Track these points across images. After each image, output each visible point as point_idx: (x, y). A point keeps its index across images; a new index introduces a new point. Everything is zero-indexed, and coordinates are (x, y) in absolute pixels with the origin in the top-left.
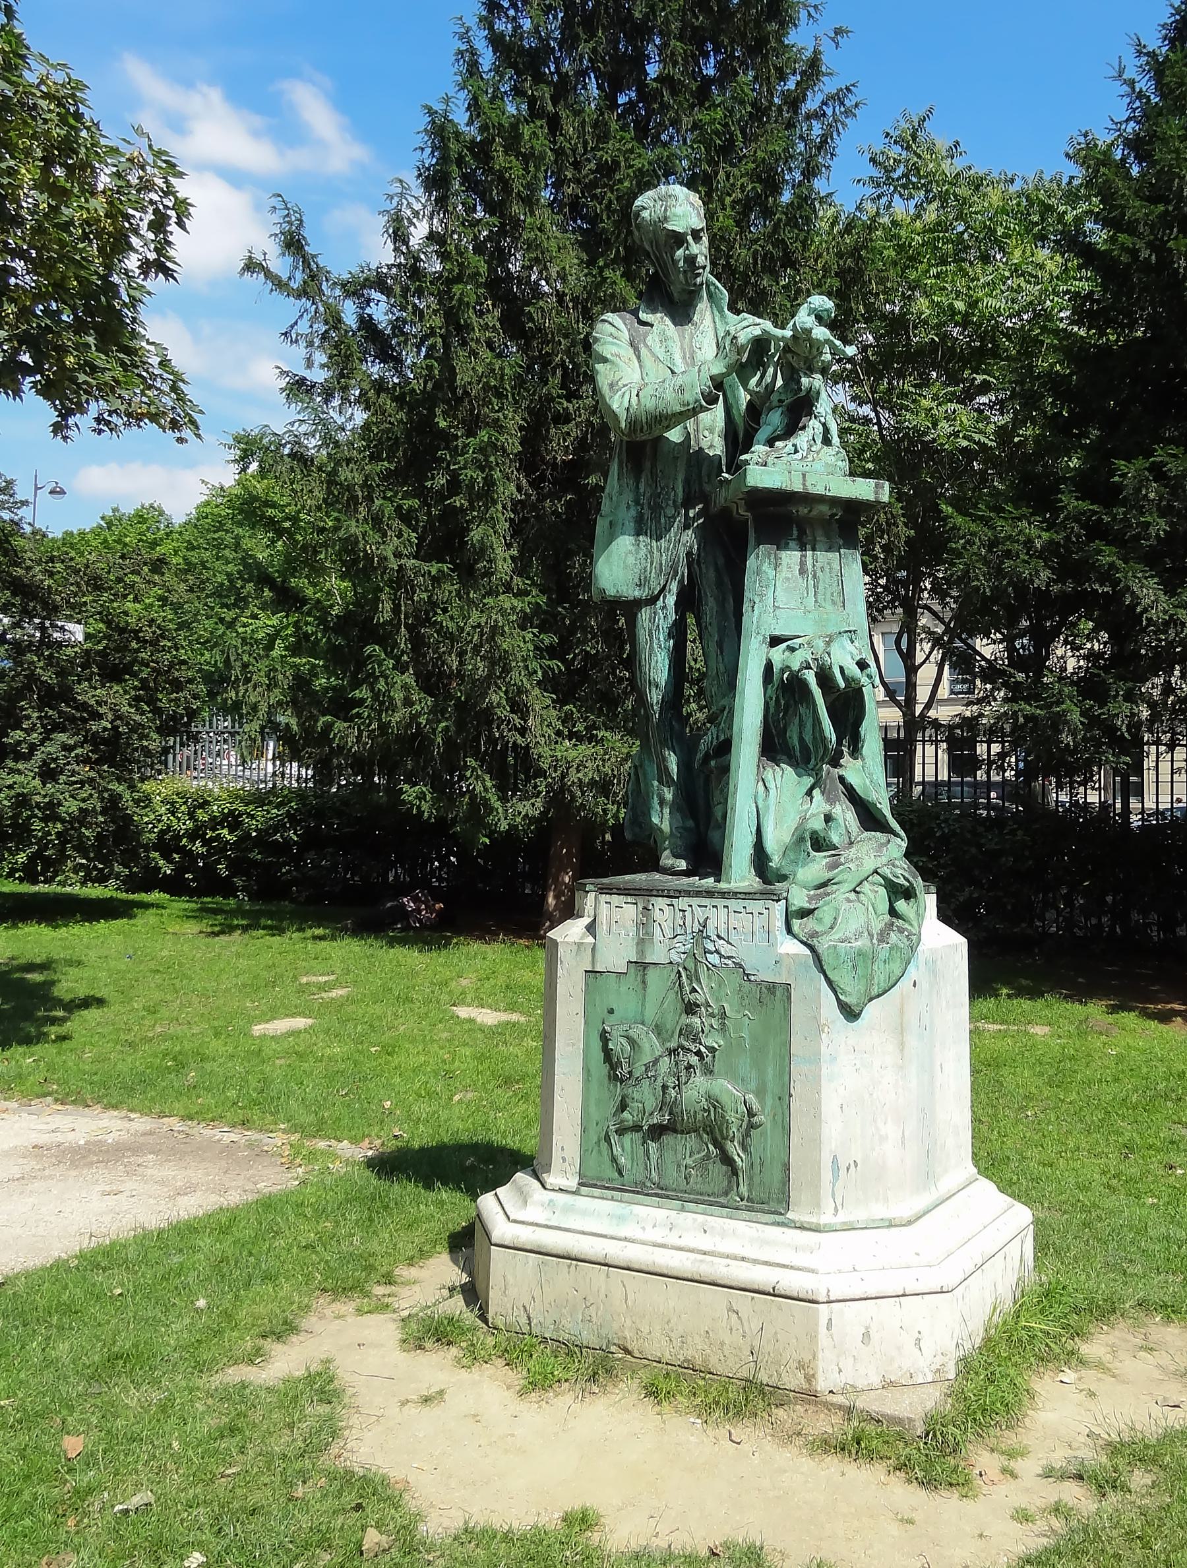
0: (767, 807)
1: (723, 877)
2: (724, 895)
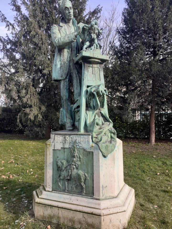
0: (87, 118)
2: (80, 135)
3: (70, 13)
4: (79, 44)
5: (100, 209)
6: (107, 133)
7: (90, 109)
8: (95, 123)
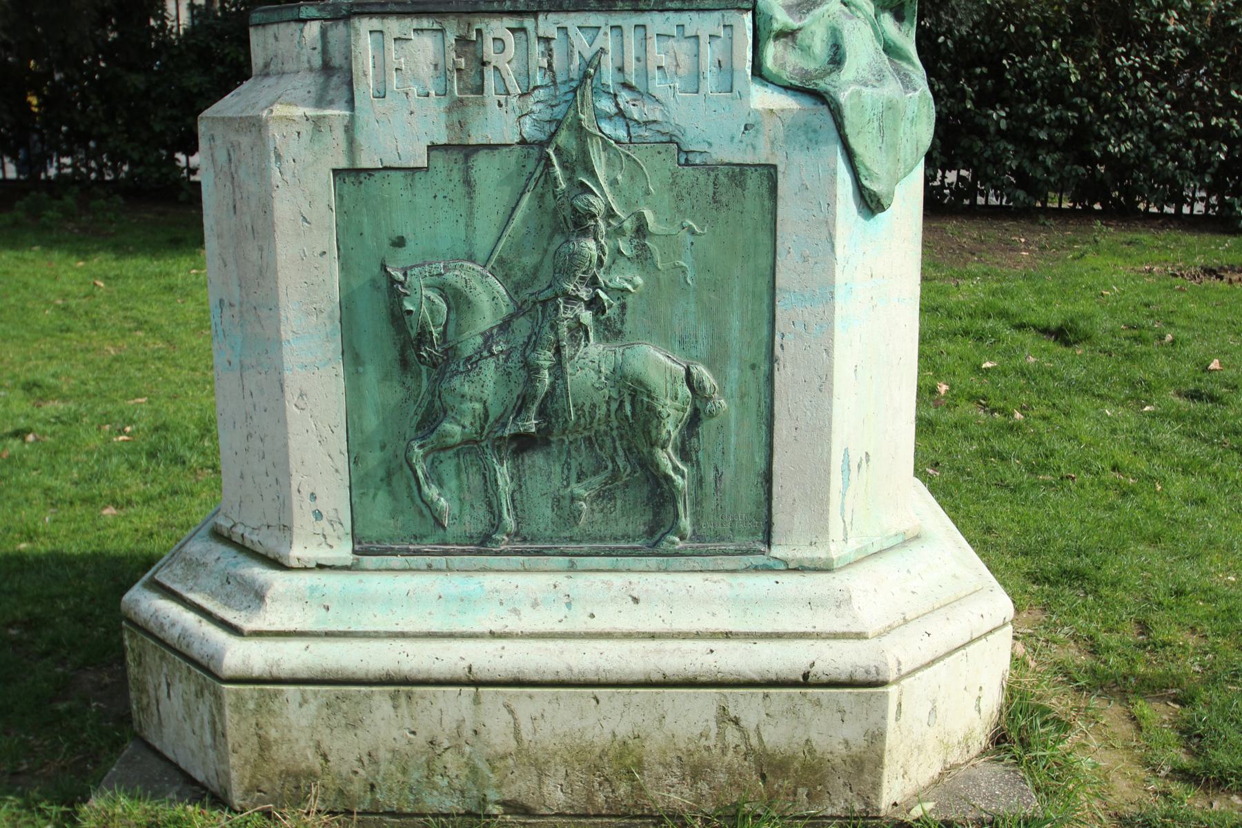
5: (860, 636)
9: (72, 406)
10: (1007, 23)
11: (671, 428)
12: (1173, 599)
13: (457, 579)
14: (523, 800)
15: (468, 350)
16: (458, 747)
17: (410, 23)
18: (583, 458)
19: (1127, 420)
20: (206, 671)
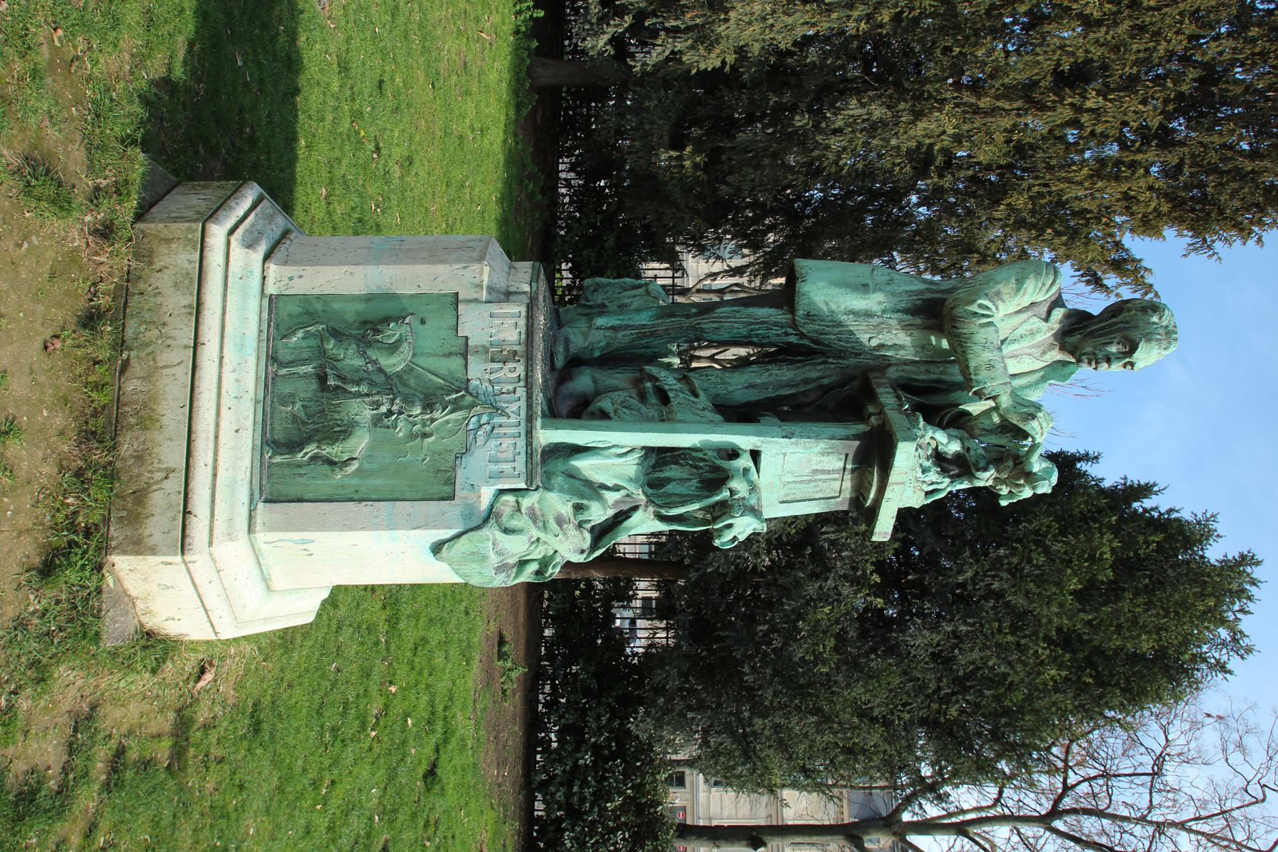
0: (608, 457)
1: (548, 421)
2: (530, 419)
3: (1109, 361)
4: (959, 393)
5: (211, 543)
6: (541, 548)
7: (652, 461)
8: (585, 502)
9: (396, 181)
10: (643, 761)
11: (327, 450)
12: (237, 782)
13: (254, 344)
14: (130, 369)
15: (369, 353)
16: (161, 336)
17: (523, 330)
18: (314, 408)
19: (369, 800)
20: (211, 216)
